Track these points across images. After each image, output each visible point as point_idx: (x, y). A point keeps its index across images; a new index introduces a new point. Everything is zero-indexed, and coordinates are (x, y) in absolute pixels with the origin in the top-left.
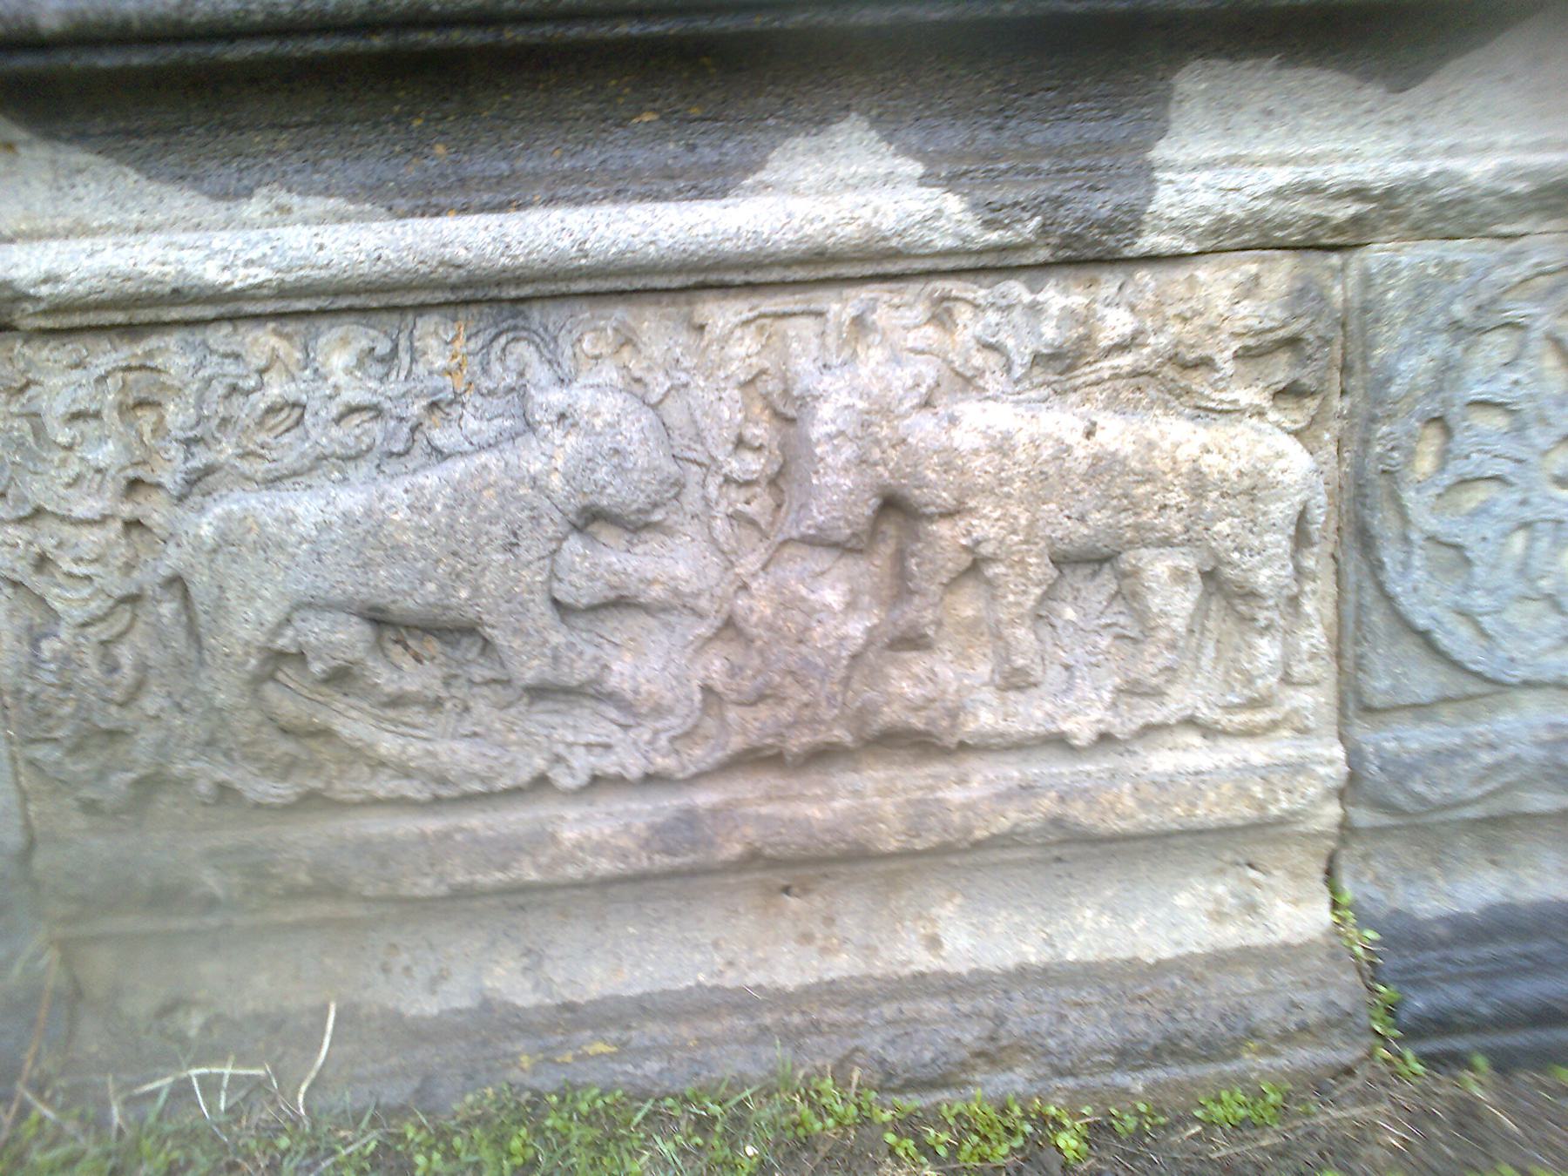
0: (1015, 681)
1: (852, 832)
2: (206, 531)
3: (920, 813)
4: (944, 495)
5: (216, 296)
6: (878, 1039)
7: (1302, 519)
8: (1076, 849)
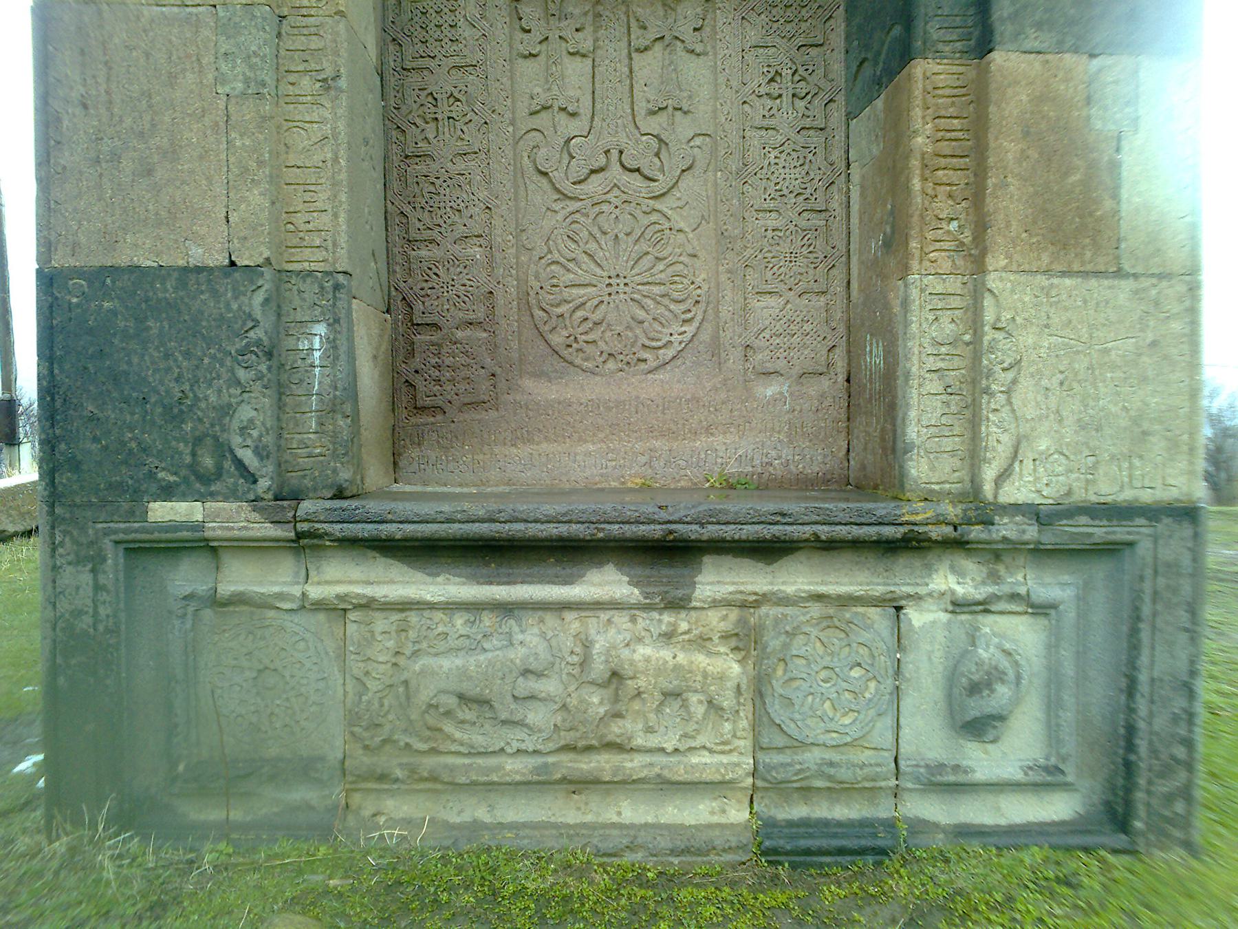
0: (649, 730)
3: (616, 770)
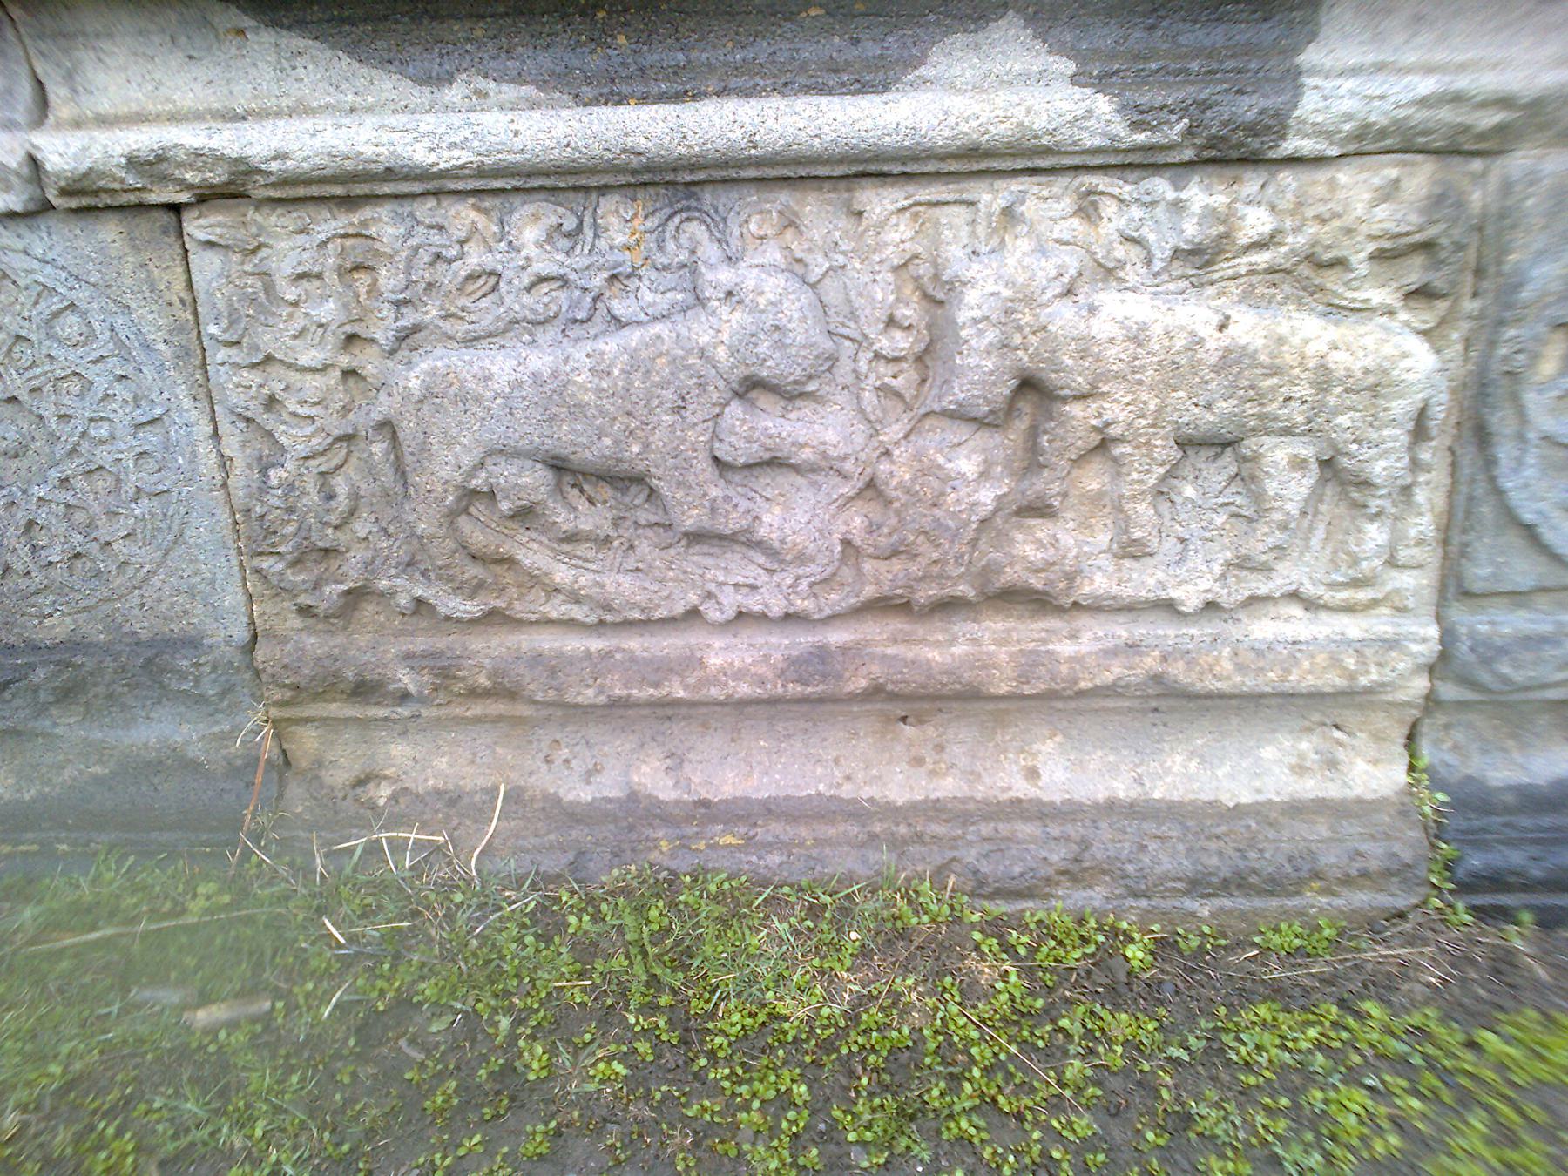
0: (1131, 550)
1: (967, 676)
2: (414, 384)
3: (1030, 663)
4: (1080, 379)
5: (423, 175)
6: (973, 852)
7: (1422, 416)
8: (1172, 702)
